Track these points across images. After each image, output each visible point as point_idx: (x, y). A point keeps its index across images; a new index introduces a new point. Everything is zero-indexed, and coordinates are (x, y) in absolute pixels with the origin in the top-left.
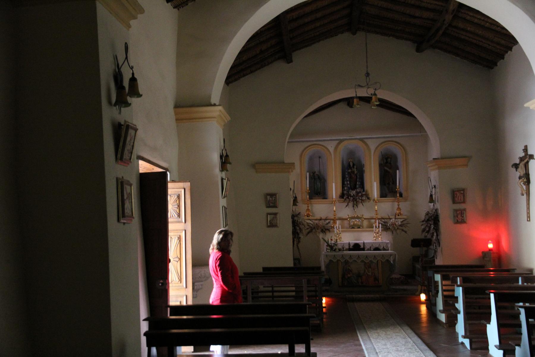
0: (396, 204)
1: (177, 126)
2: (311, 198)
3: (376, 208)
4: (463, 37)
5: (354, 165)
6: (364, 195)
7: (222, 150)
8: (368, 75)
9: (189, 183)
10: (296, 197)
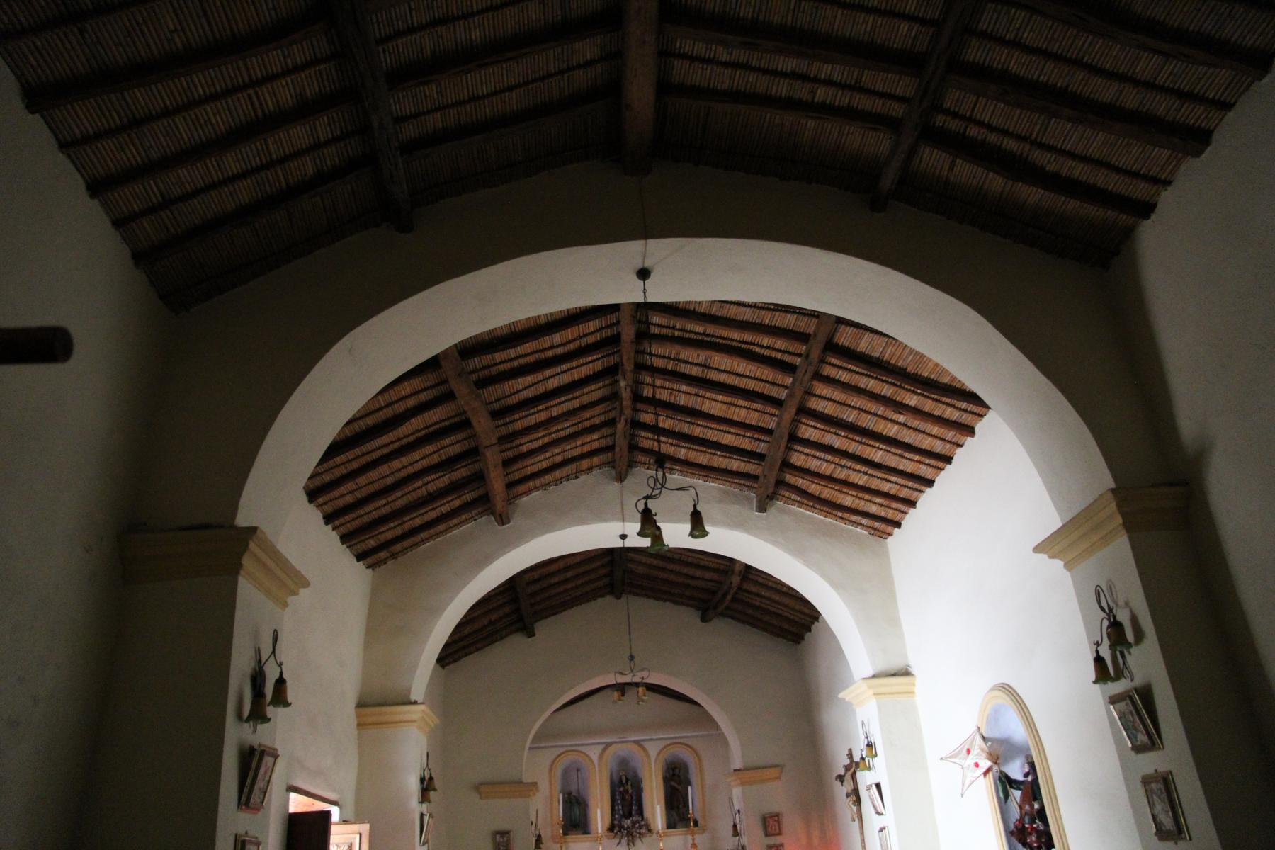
0: (690, 837)
1: (359, 734)
2: (565, 834)
3: (661, 845)
4: (758, 603)
5: (627, 780)
6: (643, 825)
7: (424, 771)
8: (632, 658)
9: (368, 825)
10: (539, 836)
